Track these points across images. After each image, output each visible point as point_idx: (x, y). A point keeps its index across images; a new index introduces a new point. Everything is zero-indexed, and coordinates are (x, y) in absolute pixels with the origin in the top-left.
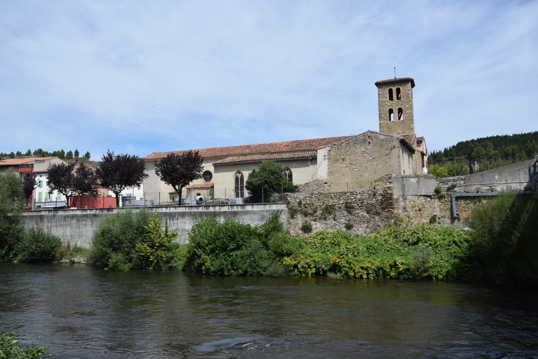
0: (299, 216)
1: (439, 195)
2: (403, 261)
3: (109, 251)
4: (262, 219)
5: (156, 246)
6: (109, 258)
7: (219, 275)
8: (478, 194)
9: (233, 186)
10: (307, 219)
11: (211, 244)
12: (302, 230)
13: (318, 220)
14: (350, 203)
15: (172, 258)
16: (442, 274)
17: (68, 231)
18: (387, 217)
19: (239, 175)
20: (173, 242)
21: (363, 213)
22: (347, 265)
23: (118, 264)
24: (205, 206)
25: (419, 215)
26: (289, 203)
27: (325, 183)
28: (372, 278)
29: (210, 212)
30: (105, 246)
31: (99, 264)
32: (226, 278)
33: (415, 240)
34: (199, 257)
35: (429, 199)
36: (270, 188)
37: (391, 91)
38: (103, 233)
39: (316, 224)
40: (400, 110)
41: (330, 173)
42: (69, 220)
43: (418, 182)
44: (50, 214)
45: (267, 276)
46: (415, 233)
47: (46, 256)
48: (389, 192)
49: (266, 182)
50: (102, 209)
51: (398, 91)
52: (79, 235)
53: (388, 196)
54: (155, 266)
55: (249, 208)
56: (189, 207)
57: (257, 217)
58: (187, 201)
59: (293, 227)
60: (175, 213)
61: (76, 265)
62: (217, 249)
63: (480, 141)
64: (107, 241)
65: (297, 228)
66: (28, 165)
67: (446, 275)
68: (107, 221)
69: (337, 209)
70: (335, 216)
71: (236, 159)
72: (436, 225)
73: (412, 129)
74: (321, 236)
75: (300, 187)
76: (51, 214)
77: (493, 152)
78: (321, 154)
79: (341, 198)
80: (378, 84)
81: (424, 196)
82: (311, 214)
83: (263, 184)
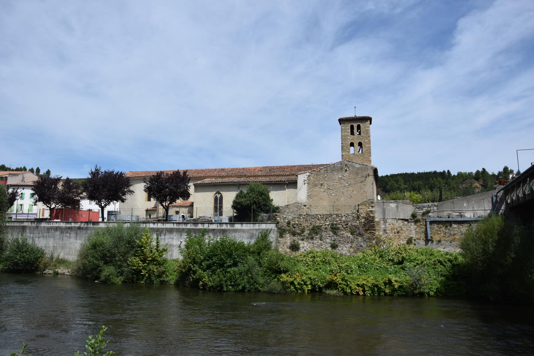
0: (288, 235)
1: (416, 219)
2: (397, 279)
3: (101, 264)
4: (251, 237)
5: (149, 260)
6: (101, 271)
7: (218, 291)
8: (450, 219)
9: (212, 205)
10: (295, 238)
11: (208, 260)
12: (290, 248)
13: (305, 240)
14: (336, 224)
15: (164, 272)
16: (433, 291)
17: (51, 243)
18: (369, 239)
19: (218, 196)
20: (164, 256)
21: (347, 234)
22: (344, 282)
23: (111, 277)
26: (278, 223)
29: (199, 230)
30: (97, 259)
31: (87, 275)
32: (225, 294)
33: (401, 260)
34: (195, 272)
35: (406, 223)
36: (258, 208)
37: (352, 127)
38: (94, 246)
41: (309, 196)
42: (53, 231)
43: (397, 207)
44: (33, 225)
45: (264, 291)
46: (399, 253)
47: (27, 267)
48: (372, 215)
49: (255, 202)
50: (87, 223)
51: (359, 127)
52: (66, 248)
53: (370, 219)
54: (146, 280)
55: (238, 226)
56: (177, 223)
57: (246, 235)
59: (282, 246)
61: (59, 276)
62: (214, 265)
63: (393, 176)
64: (99, 253)
66: (2, 177)
67: (436, 293)
68: (98, 234)
69: (324, 229)
70: (322, 236)
71: (214, 180)
72: (412, 246)
73: (370, 161)
74: (311, 255)
75: (281, 208)
76: (34, 225)
77: (403, 186)
78: (301, 178)
79: (327, 220)
80: (342, 121)
81: (402, 219)
82: (299, 234)
83: (251, 204)
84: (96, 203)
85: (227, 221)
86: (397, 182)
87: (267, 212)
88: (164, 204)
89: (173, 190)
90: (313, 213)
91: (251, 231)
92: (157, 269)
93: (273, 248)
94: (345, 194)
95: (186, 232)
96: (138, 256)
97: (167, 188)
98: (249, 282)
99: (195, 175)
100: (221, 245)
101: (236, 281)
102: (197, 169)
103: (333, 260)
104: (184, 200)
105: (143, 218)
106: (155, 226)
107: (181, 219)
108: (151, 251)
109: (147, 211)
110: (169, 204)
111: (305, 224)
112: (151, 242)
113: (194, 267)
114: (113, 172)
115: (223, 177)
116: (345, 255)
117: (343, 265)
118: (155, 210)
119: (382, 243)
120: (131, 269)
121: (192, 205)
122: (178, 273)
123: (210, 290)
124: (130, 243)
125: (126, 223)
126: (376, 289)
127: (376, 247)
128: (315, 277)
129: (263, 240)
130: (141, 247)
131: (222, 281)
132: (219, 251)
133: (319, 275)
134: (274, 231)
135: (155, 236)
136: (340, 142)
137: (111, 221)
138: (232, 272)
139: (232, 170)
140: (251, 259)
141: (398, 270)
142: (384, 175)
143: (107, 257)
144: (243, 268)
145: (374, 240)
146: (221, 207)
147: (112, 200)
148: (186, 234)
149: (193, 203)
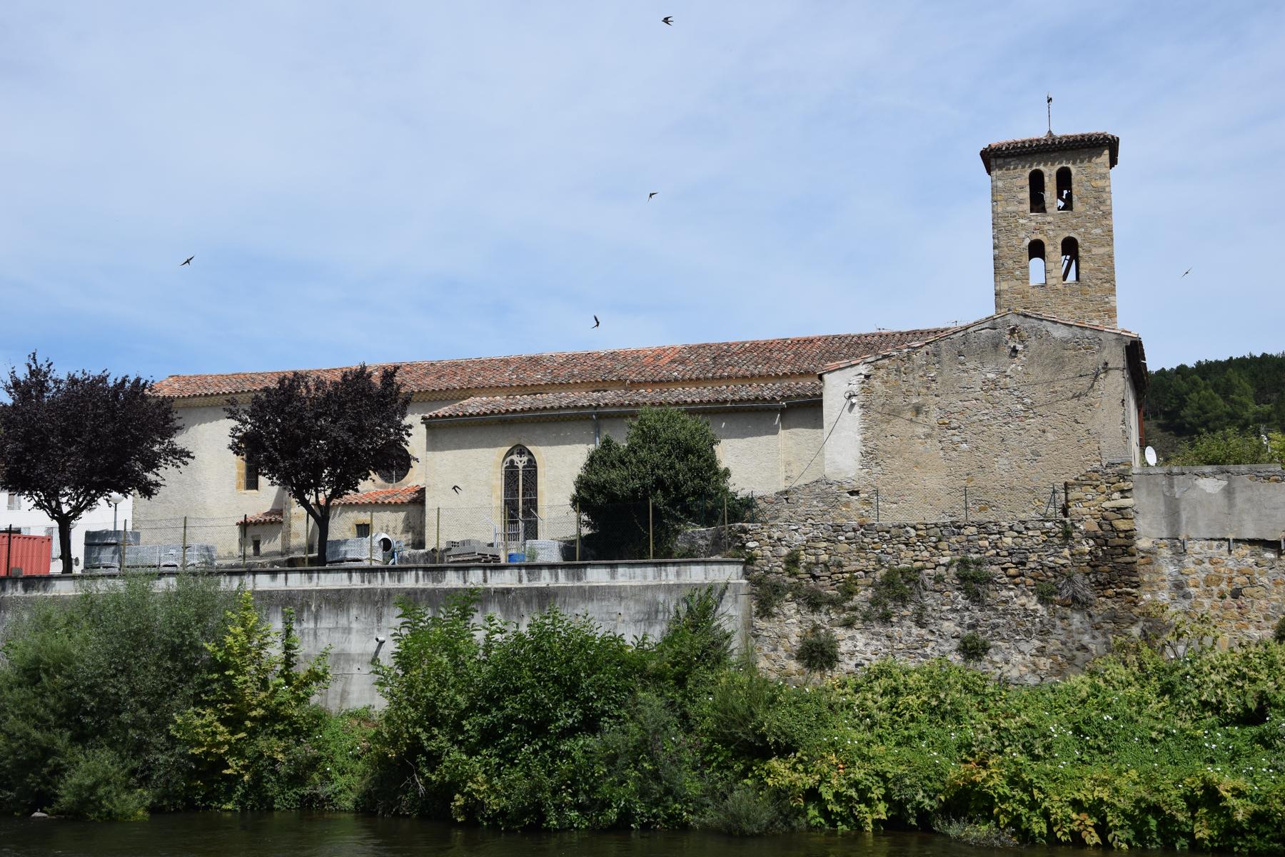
0: (790, 608)
2: (1241, 782)
3: (61, 743)
4: (650, 617)
5: (253, 719)
6: (58, 771)
7: (527, 830)
10: (820, 618)
11: (486, 711)
12: (799, 657)
13: (859, 625)
14: (978, 563)
15: (313, 764)
18: (1114, 618)
19: (520, 461)
20: (314, 700)
21: (1024, 600)
22: (1018, 794)
23: (101, 791)
24: (425, 569)
25: (1235, 611)
26: (751, 560)
27: (852, 493)
28: (1124, 846)
29: (448, 592)
30: (42, 724)
32: (554, 841)
33: (1252, 705)
34: (434, 759)
35: (1270, 555)
36: (672, 504)
39: (852, 638)
40: (1070, 247)
41: (870, 456)
43: (1229, 492)
45: (706, 829)
46: (1244, 677)
48: (1122, 525)
49: (660, 483)
51: (1064, 179)
53: (1117, 541)
54: (245, 796)
55: (597, 576)
56: (362, 570)
57: (630, 609)
59: (768, 648)
62: (507, 728)
63: (1206, 369)
64: (52, 701)
68: (46, 623)
69: (930, 583)
70: (923, 608)
71: (500, 402)
73: (1111, 313)
74: (884, 682)
75: (762, 505)
78: (838, 387)
79: (943, 545)
80: (993, 158)
81: (1252, 542)
82: (833, 603)
84: (39, 505)
85: (556, 558)
86: (1226, 391)
87: (709, 518)
88: (312, 500)
89: (345, 443)
90: (886, 521)
91: (649, 595)
93: (733, 658)
94: (1012, 443)
95: (400, 603)
96: (211, 704)
97: (322, 434)
98: (643, 793)
99: (430, 383)
101: (593, 789)
102: (434, 359)
103: (969, 701)
104: (388, 479)
105: (230, 555)
106: (279, 584)
107: (379, 555)
108: (264, 684)
109: (245, 526)
110: (329, 500)
112: (262, 646)
113: (432, 737)
114: (103, 379)
115: (535, 389)
116: (1020, 683)
117: (1012, 724)
118: (275, 520)
119: (1168, 637)
120: (182, 755)
121: (419, 499)
122: (370, 762)
123: (494, 827)
125: (161, 575)
126: (1153, 823)
127: (1146, 650)
128: (900, 770)
129: (696, 627)
130: (224, 666)
131: (542, 790)
132: (526, 672)
133: (918, 762)
134: (736, 592)
135: (277, 624)
136: (990, 243)
137: (101, 571)
138: (577, 754)
139: (571, 360)
140: (651, 701)
141: (1246, 749)
142: (1170, 364)
143: (86, 713)
144: (620, 737)
145: (1134, 622)
146: (532, 504)
147: (103, 489)
148: (399, 611)
149: (422, 492)
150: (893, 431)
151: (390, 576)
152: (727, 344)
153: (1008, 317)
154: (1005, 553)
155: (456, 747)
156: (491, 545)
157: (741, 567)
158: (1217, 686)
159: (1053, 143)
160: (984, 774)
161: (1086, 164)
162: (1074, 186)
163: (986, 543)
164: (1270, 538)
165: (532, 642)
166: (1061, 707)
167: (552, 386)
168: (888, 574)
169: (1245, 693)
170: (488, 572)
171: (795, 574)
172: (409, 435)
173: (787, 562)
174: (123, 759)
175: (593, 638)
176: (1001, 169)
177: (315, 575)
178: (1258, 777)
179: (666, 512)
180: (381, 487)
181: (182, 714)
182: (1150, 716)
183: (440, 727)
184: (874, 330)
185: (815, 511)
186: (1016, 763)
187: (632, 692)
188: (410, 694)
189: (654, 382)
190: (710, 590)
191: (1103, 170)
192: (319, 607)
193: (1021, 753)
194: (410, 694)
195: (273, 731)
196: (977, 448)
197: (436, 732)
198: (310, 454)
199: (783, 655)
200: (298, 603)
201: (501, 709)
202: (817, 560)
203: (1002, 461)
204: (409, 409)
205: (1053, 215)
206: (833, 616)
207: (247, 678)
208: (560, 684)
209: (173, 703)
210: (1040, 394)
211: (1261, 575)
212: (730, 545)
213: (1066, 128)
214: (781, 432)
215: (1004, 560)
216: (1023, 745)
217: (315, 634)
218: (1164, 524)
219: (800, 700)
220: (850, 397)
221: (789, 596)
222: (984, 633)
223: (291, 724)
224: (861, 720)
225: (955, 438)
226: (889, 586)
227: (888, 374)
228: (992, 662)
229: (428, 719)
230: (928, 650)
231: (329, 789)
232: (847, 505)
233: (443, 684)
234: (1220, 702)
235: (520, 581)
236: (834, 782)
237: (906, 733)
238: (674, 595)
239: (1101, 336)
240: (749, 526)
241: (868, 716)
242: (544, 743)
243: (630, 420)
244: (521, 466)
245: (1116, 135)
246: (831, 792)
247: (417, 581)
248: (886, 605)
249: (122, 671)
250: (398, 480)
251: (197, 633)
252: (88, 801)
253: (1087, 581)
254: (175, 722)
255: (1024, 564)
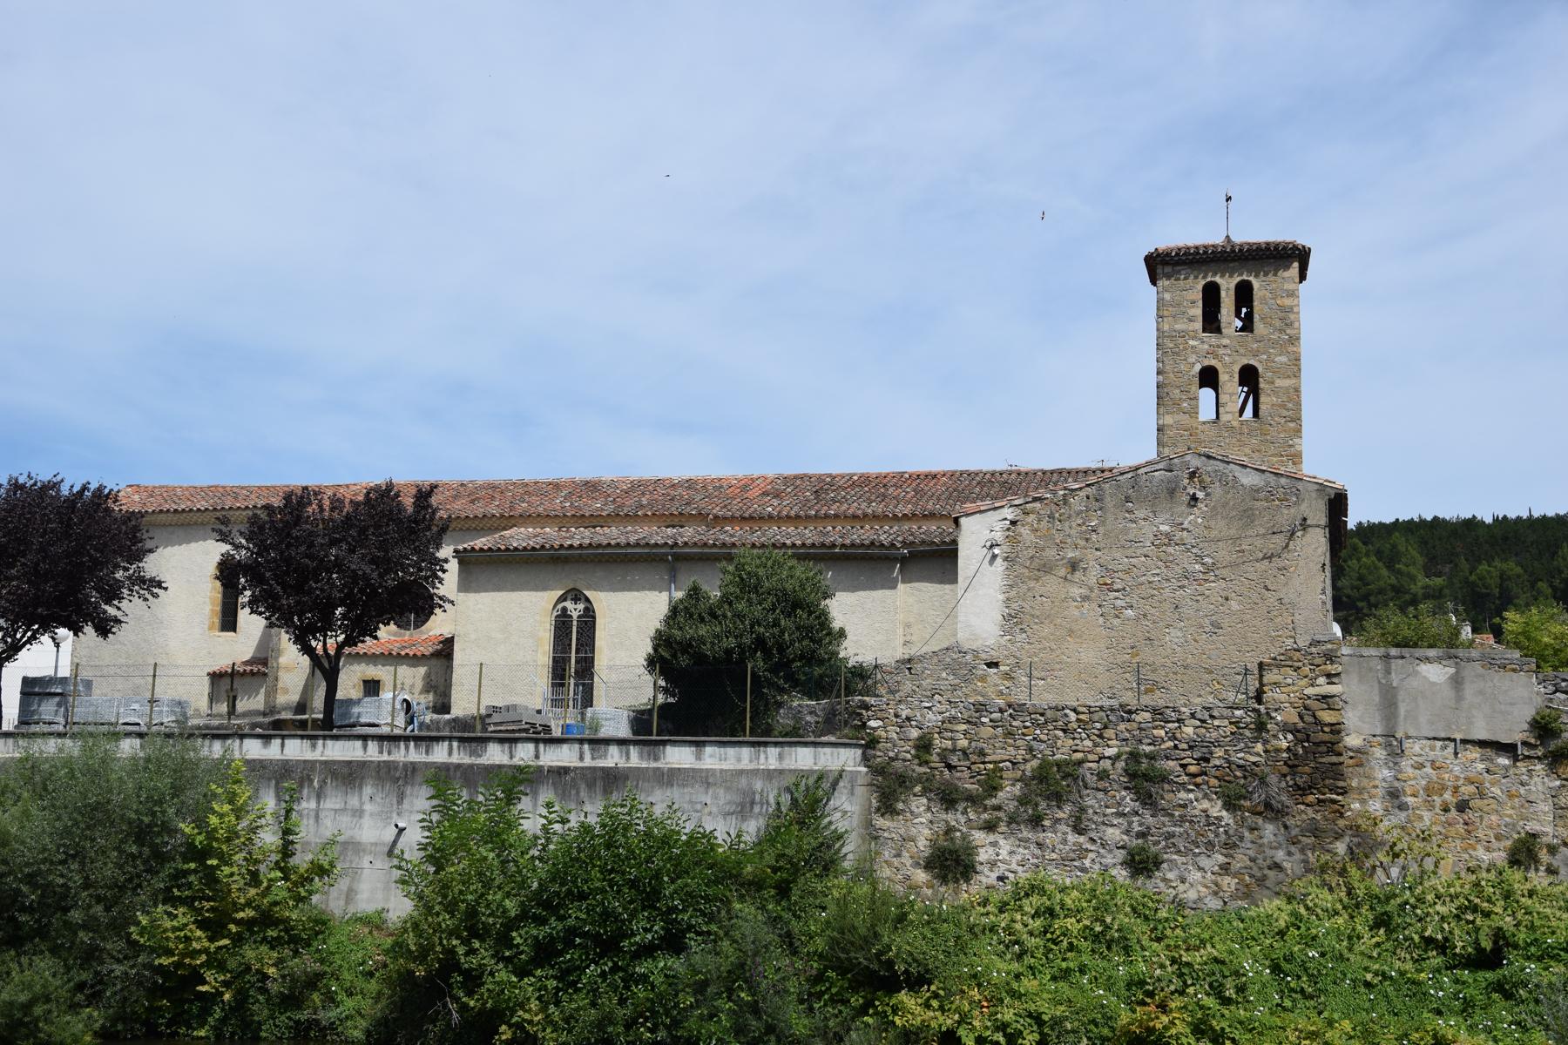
0: (919, 804)
4: (744, 808)
5: (238, 922)
9: (543, 655)
10: (955, 818)
11: (541, 921)
12: (928, 866)
13: (1003, 828)
14: (1151, 757)
15: (313, 981)
18: (1315, 831)
19: (575, 609)
20: (315, 899)
21: (1205, 804)
23: (38, 1010)
24: (461, 740)
25: (1461, 828)
26: (872, 743)
27: (991, 665)
29: (492, 770)
33: (1487, 944)
34: (473, 980)
35: (1504, 761)
36: (775, 670)
39: (994, 844)
40: (1249, 377)
41: (1013, 620)
43: (1457, 682)
48: (1327, 717)
49: (760, 643)
51: (1244, 294)
53: (1321, 737)
54: (223, 1021)
55: (678, 756)
56: (381, 738)
57: (720, 798)
58: (367, 712)
59: (889, 852)
60: (310, 765)
62: (569, 944)
65: (906, 859)
69: (1091, 780)
70: (1083, 810)
71: (550, 534)
72: (1539, 879)
73: (1296, 458)
74: (1035, 900)
77: (1422, 580)
78: (977, 534)
79: (1109, 733)
80: (1160, 265)
81: (1482, 744)
82: (973, 800)
85: (624, 731)
87: (816, 689)
88: (317, 645)
89: (366, 577)
91: (744, 782)
92: (278, 963)
93: (846, 865)
96: (188, 902)
100: (608, 846)
101: (676, 1023)
102: (466, 478)
103: (1140, 928)
106: (273, 751)
108: (254, 879)
110: (340, 647)
111: (999, 753)
112: (254, 830)
113: (471, 952)
115: (594, 521)
117: (1197, 958)
118: (260, 669)
119: (1382, 856)
121: (445, 651)
122: (387, 980)
124: (147, 834)
127: (1354, 872)
128: (1060, 1011)
129: (801, 823)
130: (201, 855)
131: (611, 1023)
132: (596, 873)
133: (1081, 1002)
134: (852, 782)
136: (1153, 366)
138: (658, 979)
139: (638, 486)
141: (1480, 999)
143: (23, 909)
145: (1338, 836)
146: (586, 669)
147: (47, 625)
148: (431, 792)
149: (449, 642)
150: (1043, 590)
151: (416, 746)
152: (830, 475)
153: (1188, 458)
154: (1185, 746)
155: (501, 965)
156: (539, 712)
157: (859, 752)
158: (1443, 919)
159: (1233, 251)
160: (1165, 1019)
161: (1271, 277)
162: (1255, 303)
163: (1162, 733)
164: (1505, 739)
165: (602, 836)
166: (1253, 938)
167: (616, 518)
168: (1040, 767)
169: (1477, 930)
170: (541, 746)
171: (927, 762)
172: (444, 571)
173: (917, 747)
174: (68, 969)
175: (678, 833)
176: (1169, 278)
177: (320, 742)
178: (1499, 1034)
179: (767, 679)
180: (395, 634)
181: (148, 913)
182: (1362, 953)
183: (482, 940)
184: (1004, 467)
185: (944, 685)
186: (1202, 1008)
187: (727, 902)
188: (445, 896)
189: (744, 519)
190: (820, 778)
191: (1291, 286)
192: (323, 783)
193: (1208, 995)
194: (445, 896)
195: (264, 939)
196: (1145, 615)
197: (477, 944)
198: (322, 590)
199: (909, 862)
200: (297, 776)
201: (561, 918)
202: (954, 745)
203: (1175, 633)
204: (446, 538)
205: (1229, 337)
206: (972, 816)
207: (235, 869)
208: (640, 892)
209: (136, 899)
210: (1224, 553)
211: (1493, 784)
212: (846, 723)
213: (1250, 233)
214: (901, 586)
215: (1183, 754)
216: (1211, 985)
217: (317, 817)
218: (1378, 717)
219: (934, 920)
220: (992, 546)
221: (918, 789)
222: (1156, 843)
223: (287, 931)
224: (1007, 947)
225: (1119, 603)
226: (1041, 782)
227: (1039, 520)
228: (1165, 880)
229: (466, 928)
230: (1087, 863)
231: (333, 1014)
232: (983, 679)
233: (487, 885)
234: (1446, 939)
235: (581, 758)
236: (976, 1023)
237: (1064, 965)
238: (775, 783)
239: (1300, 486)
240: (871, 700)
241: (1017, 942)
242: (615, 964)
243: (724, 563)
244: (575, 615)
245: (1308, 245)
246: (972, 1036)
247: (450, 753)
248: (1037, 805)
249: (73, 857)
250: (417, 627)
251: (171, 811)
252: (21, 1023)
253: (1283, 784)
254: (138, 923)
255: (1207, 760)
